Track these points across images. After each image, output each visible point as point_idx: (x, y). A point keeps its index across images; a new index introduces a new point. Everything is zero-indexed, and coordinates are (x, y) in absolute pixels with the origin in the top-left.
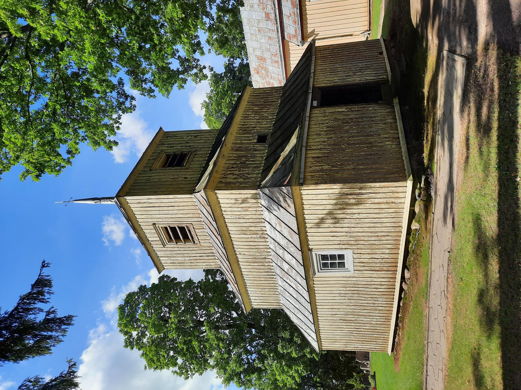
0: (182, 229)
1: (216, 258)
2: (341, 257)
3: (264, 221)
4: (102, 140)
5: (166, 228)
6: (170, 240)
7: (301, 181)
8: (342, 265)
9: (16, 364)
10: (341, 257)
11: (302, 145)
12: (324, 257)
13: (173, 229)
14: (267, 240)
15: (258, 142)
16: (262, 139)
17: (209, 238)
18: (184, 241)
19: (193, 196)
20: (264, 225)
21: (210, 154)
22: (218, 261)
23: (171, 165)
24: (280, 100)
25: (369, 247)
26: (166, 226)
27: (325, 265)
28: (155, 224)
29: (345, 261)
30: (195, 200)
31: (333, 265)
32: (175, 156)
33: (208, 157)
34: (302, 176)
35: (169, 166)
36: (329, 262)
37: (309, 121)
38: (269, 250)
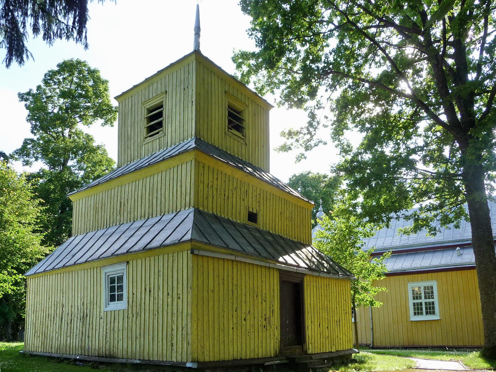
0: (160, 125)
1: (129, 163)
2: (120, 298)
3: (162, 214)
4: (83, 158)
5: (161, 107)
6: (150, 111)
7: (196, 252)
8: (112, 298)
9: (61, 61)
10: (120, 298)
11: (238, 256)
12: (120, 279)
13: (160, 115)
14: (143, 218)
15: (249, 212)
16: (252, 217)
17: (150, 155)
18: (148, 127)
19: (193, 137)
20: (158, 215)
21: (242, 160)
22: (125, 165)
23: (230, 114)
24: (296, 240)
25: (130, 327)
26: (164, 107)
27: (112, 281)
28: (166, 93)
29: (116, 302)
30: (189, 139)
31: (112, 289)
32: (241, 120)
33: (234, 155)
34: (201, 253)
35: (229, 113)
36: (116, 293)
37: (266, 267)
38: (132, 221)
